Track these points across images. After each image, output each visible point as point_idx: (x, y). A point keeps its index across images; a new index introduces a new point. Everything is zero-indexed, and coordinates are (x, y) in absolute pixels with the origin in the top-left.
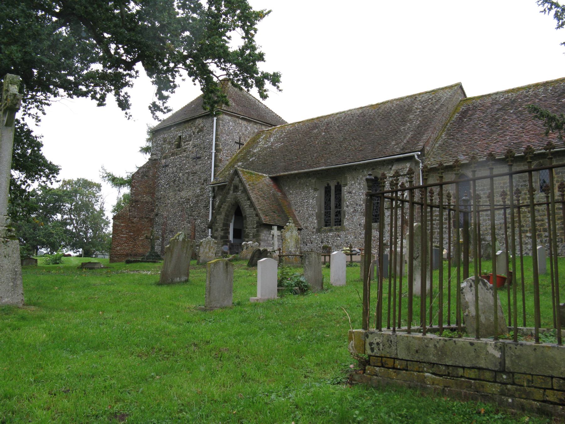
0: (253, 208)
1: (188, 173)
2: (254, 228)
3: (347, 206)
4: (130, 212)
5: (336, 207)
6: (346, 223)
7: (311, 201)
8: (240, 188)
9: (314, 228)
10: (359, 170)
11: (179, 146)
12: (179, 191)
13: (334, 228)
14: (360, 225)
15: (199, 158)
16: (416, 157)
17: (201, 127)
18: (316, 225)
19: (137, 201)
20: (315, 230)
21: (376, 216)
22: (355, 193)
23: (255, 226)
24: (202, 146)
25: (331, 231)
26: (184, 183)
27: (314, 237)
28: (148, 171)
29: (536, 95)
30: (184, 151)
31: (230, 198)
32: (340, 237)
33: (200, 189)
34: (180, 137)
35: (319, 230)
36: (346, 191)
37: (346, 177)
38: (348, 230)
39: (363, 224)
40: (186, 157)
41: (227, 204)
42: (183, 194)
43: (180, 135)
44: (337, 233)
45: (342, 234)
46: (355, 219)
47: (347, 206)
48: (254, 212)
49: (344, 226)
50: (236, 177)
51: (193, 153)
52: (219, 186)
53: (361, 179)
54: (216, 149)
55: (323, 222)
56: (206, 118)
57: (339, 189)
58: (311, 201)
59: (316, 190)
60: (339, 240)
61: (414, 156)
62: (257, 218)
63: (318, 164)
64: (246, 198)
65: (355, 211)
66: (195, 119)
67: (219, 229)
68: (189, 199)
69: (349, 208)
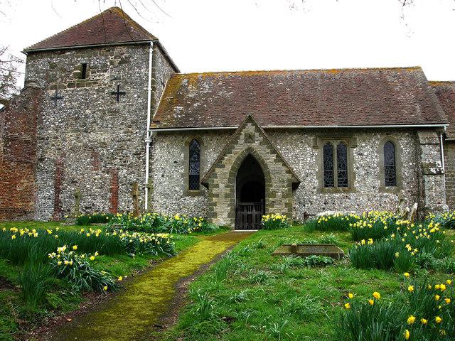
2: (284, 186)
3: (357, 168)
4: (5, 154)
5: (339, 167)
11: (83, 75)
12: (86, 131)
13: (341, 189)
15: (124, 93)
16: (445, 128)
19: (14, 140)
25: (337, 192)
27: (315, 197)
28: (27, 102)
29: (296, 76)
31: (240, 149)
32: (349, 199)
33: (125, 133)
34: (84, 66)
35: (321, 191)
37: (355, 139)
40: (98, 91)
42: (92, 136)
43: (84, 62)
45: (353, 196)
48: (284, 168)
50: (249, 124)
54: (152, 87)
57: (343, 154)
58: (309, 159)
59: (315, 147)
61: (443, 127)
62: (289, 176)
63: (195, 125)
65: (367, 173)
66: (63, 51)
67: (222, 186)
69: (360, 169)
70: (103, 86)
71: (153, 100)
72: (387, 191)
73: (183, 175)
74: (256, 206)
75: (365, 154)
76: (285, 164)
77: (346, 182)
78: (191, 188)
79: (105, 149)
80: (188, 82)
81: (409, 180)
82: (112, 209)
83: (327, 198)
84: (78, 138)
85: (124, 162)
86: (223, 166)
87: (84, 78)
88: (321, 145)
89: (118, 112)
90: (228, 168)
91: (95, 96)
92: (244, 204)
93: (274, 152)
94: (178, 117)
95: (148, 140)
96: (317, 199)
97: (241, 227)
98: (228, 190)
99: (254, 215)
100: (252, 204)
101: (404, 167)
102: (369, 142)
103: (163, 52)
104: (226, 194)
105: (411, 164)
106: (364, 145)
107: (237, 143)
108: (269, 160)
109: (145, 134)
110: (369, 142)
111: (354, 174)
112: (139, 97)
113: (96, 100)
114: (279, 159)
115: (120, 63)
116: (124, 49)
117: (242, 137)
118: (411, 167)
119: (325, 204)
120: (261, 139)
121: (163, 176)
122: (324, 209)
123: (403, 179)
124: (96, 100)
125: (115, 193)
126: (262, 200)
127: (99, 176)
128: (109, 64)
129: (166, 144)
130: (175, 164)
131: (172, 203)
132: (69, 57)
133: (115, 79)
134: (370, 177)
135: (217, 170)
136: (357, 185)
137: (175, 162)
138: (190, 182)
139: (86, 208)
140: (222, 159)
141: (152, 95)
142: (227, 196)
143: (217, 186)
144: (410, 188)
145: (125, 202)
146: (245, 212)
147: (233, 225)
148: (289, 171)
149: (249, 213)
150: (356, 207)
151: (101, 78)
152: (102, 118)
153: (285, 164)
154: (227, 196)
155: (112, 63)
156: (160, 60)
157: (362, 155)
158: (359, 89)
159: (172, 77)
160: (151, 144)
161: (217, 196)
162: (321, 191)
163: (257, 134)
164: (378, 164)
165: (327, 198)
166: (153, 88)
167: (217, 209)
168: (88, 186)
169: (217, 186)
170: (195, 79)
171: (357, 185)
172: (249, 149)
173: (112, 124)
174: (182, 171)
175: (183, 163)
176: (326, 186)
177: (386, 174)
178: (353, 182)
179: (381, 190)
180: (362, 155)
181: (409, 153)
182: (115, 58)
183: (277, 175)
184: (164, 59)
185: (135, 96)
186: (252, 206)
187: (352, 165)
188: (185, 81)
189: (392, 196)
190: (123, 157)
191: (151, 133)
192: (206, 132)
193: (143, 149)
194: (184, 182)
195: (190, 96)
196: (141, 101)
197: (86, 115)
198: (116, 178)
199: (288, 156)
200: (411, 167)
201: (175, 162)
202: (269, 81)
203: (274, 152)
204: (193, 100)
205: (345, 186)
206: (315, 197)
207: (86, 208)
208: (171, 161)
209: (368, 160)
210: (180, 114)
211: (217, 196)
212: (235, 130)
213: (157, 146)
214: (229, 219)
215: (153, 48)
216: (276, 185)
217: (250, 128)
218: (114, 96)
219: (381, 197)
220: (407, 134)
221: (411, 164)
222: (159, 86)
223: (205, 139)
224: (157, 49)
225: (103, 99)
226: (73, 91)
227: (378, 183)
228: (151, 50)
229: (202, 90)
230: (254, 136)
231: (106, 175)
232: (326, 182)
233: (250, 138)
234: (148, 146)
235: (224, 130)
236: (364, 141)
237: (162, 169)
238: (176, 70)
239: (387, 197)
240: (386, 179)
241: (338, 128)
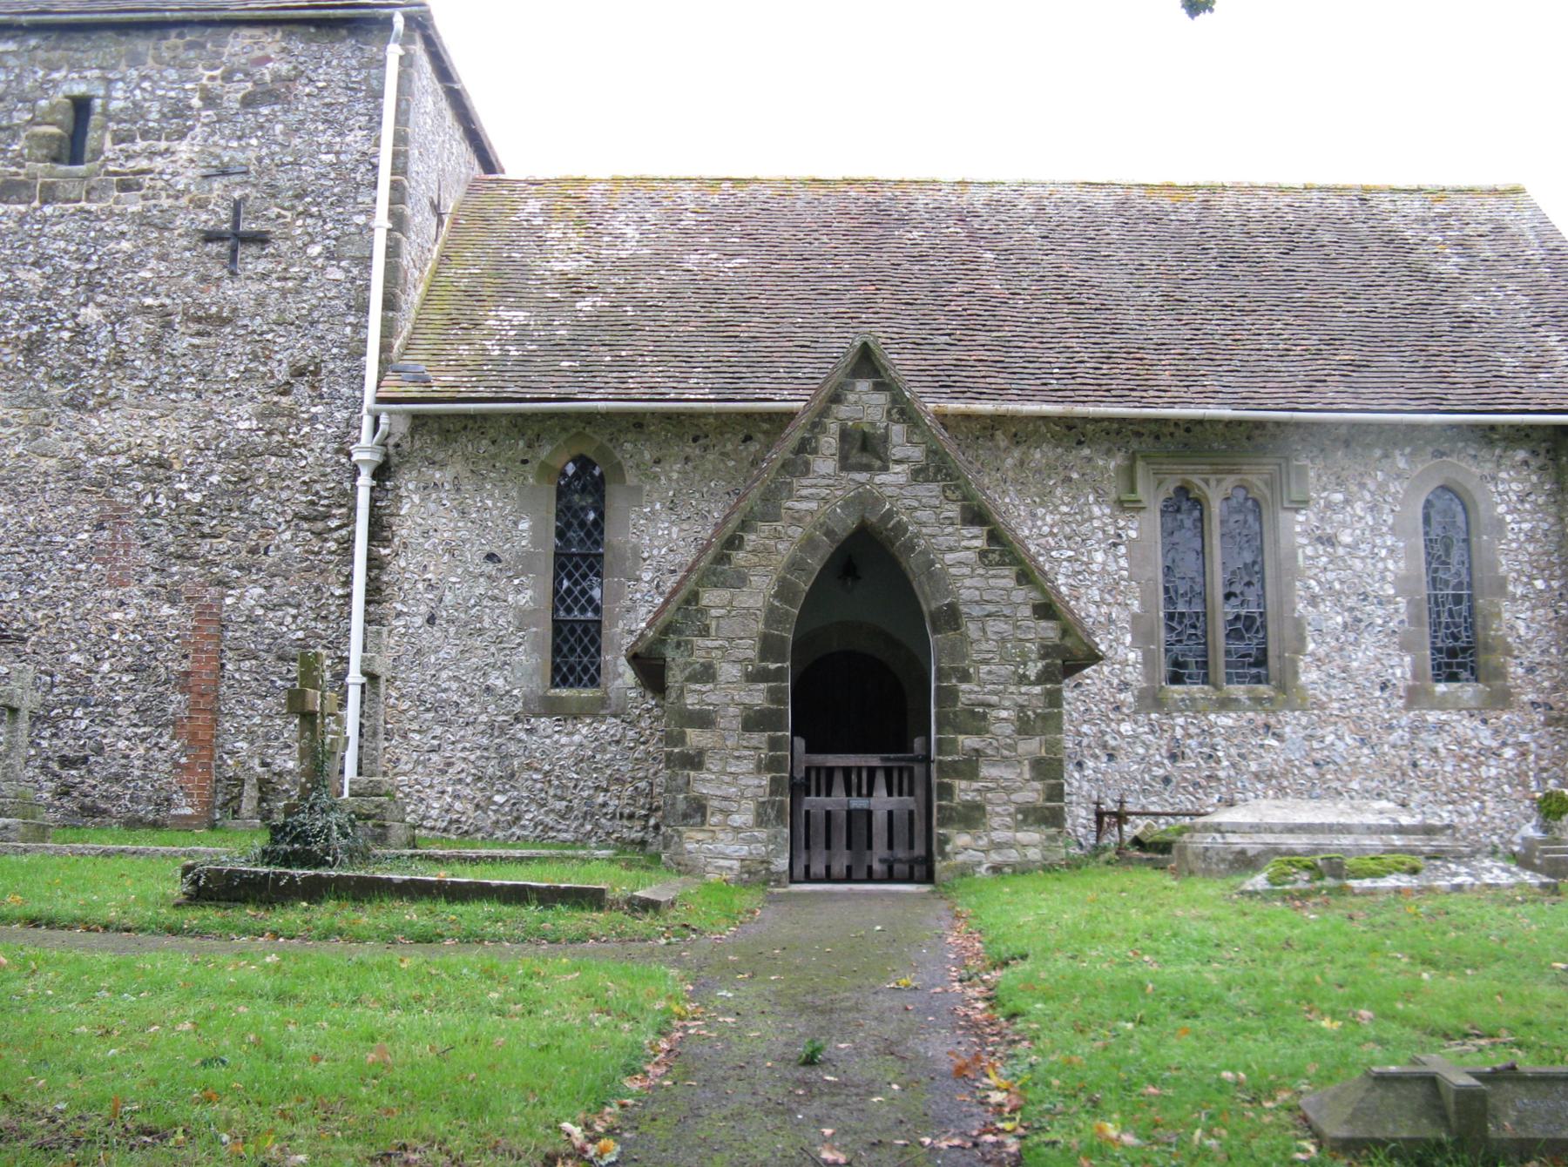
0: (1010, 572)
1: (165, 315)
2: (1023, 679)
3: (1313, 601)
6: (1309, 676)
7: (1099, 557)
8: (897, 453)
9: (1125, 686)
10: (1369, 446)
12: (77, 404)
13: (1239, 691)
14: (1384, 687)
15: (261, 239)
17: (277, 77)
18: (1134, 676)
20: (1127, 697)
21: (1452, 653)
22: (1353, 548)
23: (1033, 670)
24: (283, 180)
25: (1225, 704)
26: (119, 362)
27: (1126, 728)
30: (125, 187)
31: (821, 495)
32: (1279, 737)
33: (262, 416)
34: (81, 106)
35: (1151, 700)
36: (1305, 533)
38: (1322, 707)
39: (1401, 685)
40: (143, 220)
41: (797, 532)
43: (80, 89)
44: (1261, 718)
45: (1292, 723)
46: (1359, 659)
47: (1313, 601)
49: (1303, 688)
50: (863, 385)
51: (201, 205)
52: (415, 416)
53: (1382, 487)
55: (1164, 668)
56: (309, 40)
58: (1099, 557)
60: (1273, 753)
62: (1048, 630)
63: (1139, 388)
64: (953, 510)
65: (1355, 624)
67: (729, 671)
68: (161, 464)
70: (166, 203)
71: (393, 272)
72: (1441, 704)
73: (524, 619)
74: (888, 772)
75: (1346, 538)
76: (1026, 576)
77: (1261, 661)
78: (562, 674)
79: (163, 490)
80: (546, 211)
81: (1533, 655)
82: (184, 767)
83: (1179, 733)
84: (37, 435)
85: (253, 551)
86: (741, 580)
87: (76, 158)
88: (1152, 496)
89: (226, 322)
90: (758, 593)
91: (125, 245)
92: (832, 760)
93: (976, 515)
94: (505, 353)
95: (365, 452)
96: (1136, 737)
97: (818, 868)
98: (758, 696)
99: (879, 820)
100: (874, 760)
101: (1514, 599)
102: (1362, 486)
103: (443, 72)
104: (747, 707)
105: (1540, 584)
106: (1338, 497)
107: (806, 470)
108: (952, 556)
109: (352, 425)
110: (1362, 486)
111: (1299, 624)
112: (330, 255)
113: (132, 262)
114: (1002, 548)
115: (248, 102)
116: (272, 42)
117: (829, 442)
118: (1540, 600)
119: (1173, 757)
120: (917, 453)
121: (431, 620)
122: (1166, 780)
123: (1508, 651)
124: (132, 262)
125: (207, 701)
126: (918, 743)
127: (133, 614)
128: (196, 102)
129: (449, 473)
130: (490, 568)
131: (464, 748)
132: (11, 62)
133: (224, 172)
134: (1367, 639)
135: (709, 597)
136: (1314, 675)
137: (491, 557)
138: (556, 650)
139: (66, 762)
140: (734, 542)
141: (393, 251)
142: (754, 721)
143: (707, 674)
144: (1541, 691)
145: (251, 737)
146: (838, 801)
147: (782, 863)
148: (1046, 610)
149: (858, 803)
150: (1310, 771)
151: (159, 163)
152: (155, 347)
153: (1026, 576)
154: (754, 721)
155: (210, 100)
156: (430, 107)
157: (1330, 541)
158: (1287, 263)
159: (473, 188)
160: (381, 473)
161: (703, 720)
162: (1151, 700)
163: (898, 431)
164: (1402, 584)
165: (1179, 733)
166: (398, 221)
167: (705, 784)
168: (75, 658)
169: (707, 674)
170: (575, 201)
171: (1314, 675)
172: (865, 500)
173: (203, 376)
174: (525, 598)
175: (526, 563)
176: (1176, 679)
177: (1436, 625)
178: (1294, 663)
179: (1415, 697)
180: (1330, 541)
181: (1530, 538)
182: (228, 77)
183: (995, 626)
184: (444, 104)
185: (315, 250)
186: (872, 771)
187: (1291, 586)
188: (533, 206)
189: (1465, 726)
190: (250, 527)
191: (384, 419)
192: (637, 423)
193: (344, 494)
194: (525, 664)
195: (558, 267)
196: (340, 275)
197: (79, 331)
198: (212, 620)
199: (1036, 525)
200: (1540, 600)
201: (491, 557)
202: (902, 221)
203: (976, 515)
204: (574, 286)
205: (1258, 679)
206: (1126, 728)
207: (66, 762)
208: (472, 557)
209: (1358, 564)
210: (518, 342)
211: (703, 720)
212: (791, 415)
213: (407, 481)
214: (761, 834)
215: (406, 41)
216: (987, 666)
217: (866, 405)
218: (214, 248)
219: (1415, 731)
220: (1521, 455)
221: (1540, 584)
222: (419, 217)
223: (629, 451)
224: (418, 48)
225: (163, 258)
226: (22, 220)
227: (1401, 669)
228: (394, 51)
229: (611, 246)
230: (885, 438)
231: (166, 610)
232: (1176, 664)
233: (864, 448)
234: (365, 481)
235: (718, 415)
236: (1340, 483)
237: (431, 587)
238: (488, 163)
239: (1440, 727)
240: (1436, 650)
241: (1230, 424)
